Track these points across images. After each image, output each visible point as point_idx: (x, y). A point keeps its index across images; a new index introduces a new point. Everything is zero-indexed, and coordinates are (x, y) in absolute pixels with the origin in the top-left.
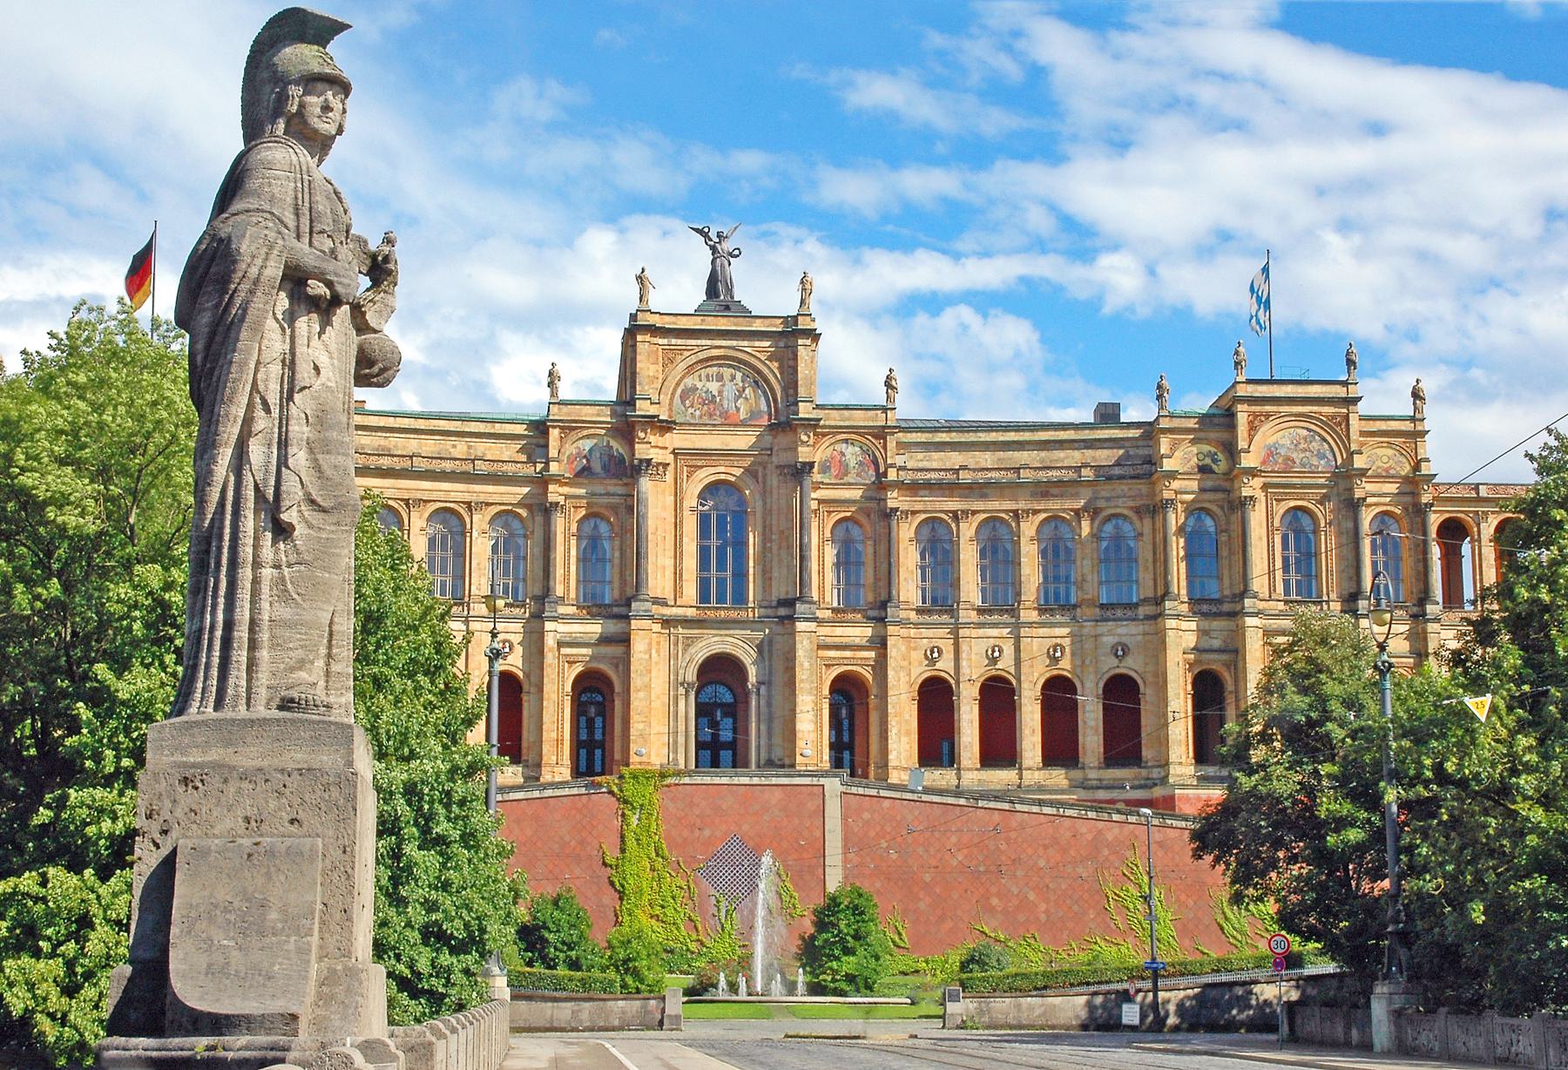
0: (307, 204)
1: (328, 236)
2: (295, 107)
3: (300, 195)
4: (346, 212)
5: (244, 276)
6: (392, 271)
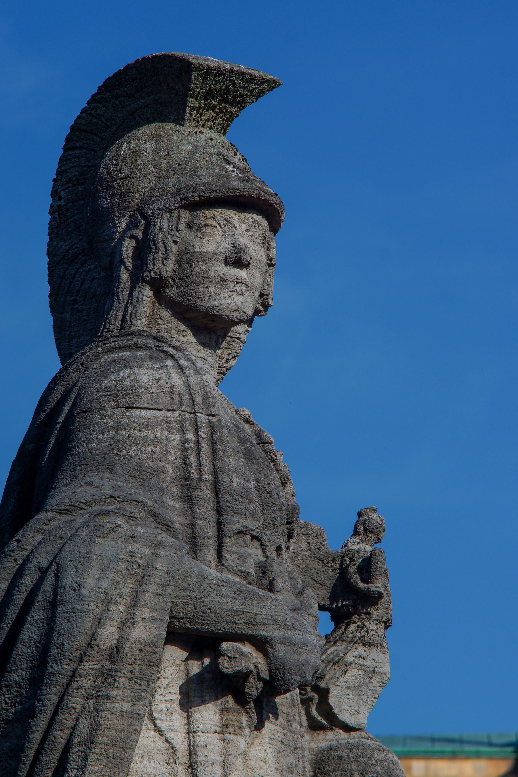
0: (208, 477)
1: (253, 537)
2: (170, 265)
3: (193, 458)
4: (284, 484)
5: (90, 646)
6: (380, 595)
